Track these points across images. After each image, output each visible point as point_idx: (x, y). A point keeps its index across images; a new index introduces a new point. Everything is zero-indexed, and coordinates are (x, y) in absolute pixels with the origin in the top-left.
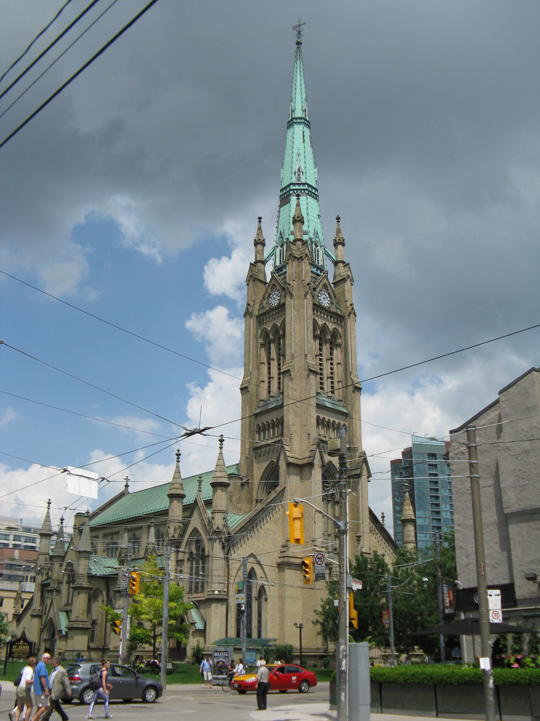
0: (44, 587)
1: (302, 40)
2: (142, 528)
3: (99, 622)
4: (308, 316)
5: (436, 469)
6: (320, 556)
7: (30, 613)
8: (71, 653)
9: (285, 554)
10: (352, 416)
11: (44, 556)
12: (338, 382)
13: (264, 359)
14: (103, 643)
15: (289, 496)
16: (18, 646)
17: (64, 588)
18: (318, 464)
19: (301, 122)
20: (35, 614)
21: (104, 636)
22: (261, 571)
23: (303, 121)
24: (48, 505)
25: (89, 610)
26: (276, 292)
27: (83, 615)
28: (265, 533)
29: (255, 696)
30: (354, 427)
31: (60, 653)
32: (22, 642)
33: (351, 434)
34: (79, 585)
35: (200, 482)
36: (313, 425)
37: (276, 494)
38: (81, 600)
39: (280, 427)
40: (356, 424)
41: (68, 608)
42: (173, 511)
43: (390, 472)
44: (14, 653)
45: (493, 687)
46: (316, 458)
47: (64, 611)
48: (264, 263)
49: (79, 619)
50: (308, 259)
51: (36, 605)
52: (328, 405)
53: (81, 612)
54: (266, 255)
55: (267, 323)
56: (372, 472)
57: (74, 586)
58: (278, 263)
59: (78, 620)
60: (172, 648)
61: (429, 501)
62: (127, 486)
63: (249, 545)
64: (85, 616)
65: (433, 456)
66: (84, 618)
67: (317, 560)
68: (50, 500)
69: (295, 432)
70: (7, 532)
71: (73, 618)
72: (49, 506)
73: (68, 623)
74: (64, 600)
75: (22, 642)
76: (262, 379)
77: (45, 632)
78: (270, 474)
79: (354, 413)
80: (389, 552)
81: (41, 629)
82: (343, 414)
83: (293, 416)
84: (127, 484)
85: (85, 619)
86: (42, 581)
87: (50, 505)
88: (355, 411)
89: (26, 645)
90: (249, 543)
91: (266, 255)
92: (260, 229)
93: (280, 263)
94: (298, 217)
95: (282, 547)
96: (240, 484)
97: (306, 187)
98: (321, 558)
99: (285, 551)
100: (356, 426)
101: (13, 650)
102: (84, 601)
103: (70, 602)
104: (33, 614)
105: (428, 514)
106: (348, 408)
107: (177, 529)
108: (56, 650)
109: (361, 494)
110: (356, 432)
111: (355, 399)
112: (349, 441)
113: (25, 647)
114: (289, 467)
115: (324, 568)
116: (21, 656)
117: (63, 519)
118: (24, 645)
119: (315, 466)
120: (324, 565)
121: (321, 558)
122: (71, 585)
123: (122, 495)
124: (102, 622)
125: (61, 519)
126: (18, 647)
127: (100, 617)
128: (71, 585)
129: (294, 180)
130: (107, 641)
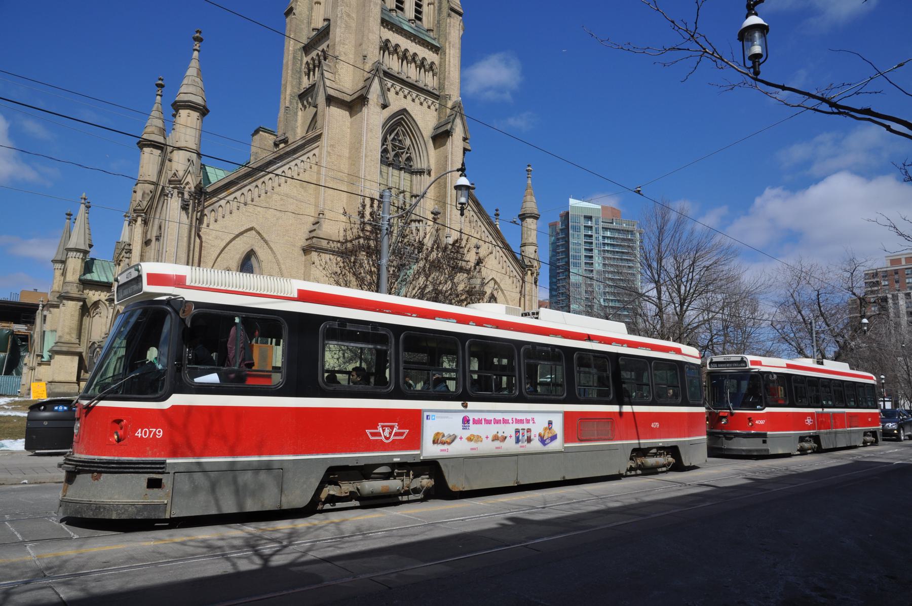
5: (591, 221)
9: (314, 234)
10: (445, 51)
15: (327, 147)
18: (375, 100)
22: (271, 257)
27: (69, 334)
28: (282, 199)
29: (890, 408)
30: (447, 66)
33: (442, 76)
36: (372, 44)
37: (304, 141)
40: (450, 62)
42: (142, 167)
43: (631, 411)
45: (622, 372)
46: (372, 89)
49: (63, 340)
52: (406, 28)
53: (67, 330)
61: (583, 260)
63: (247, 214)
65: (589, 218)
69: (344, 53)
80: (508, 268)
82: (419, 42)
83: (343, 30)
90: (246, 211)
95: (313, 225)
96: (271, 143)
99: (315, 230)
100: (449, 65)
102: (72, 315)
105: (581, 272)
106: (441, 40)
107: (148, 194)
109: (452, 160)
110: (449, 73)
111: (450, 26)
112: (439, 88)
114: (330, 103)
119: (371, 102)
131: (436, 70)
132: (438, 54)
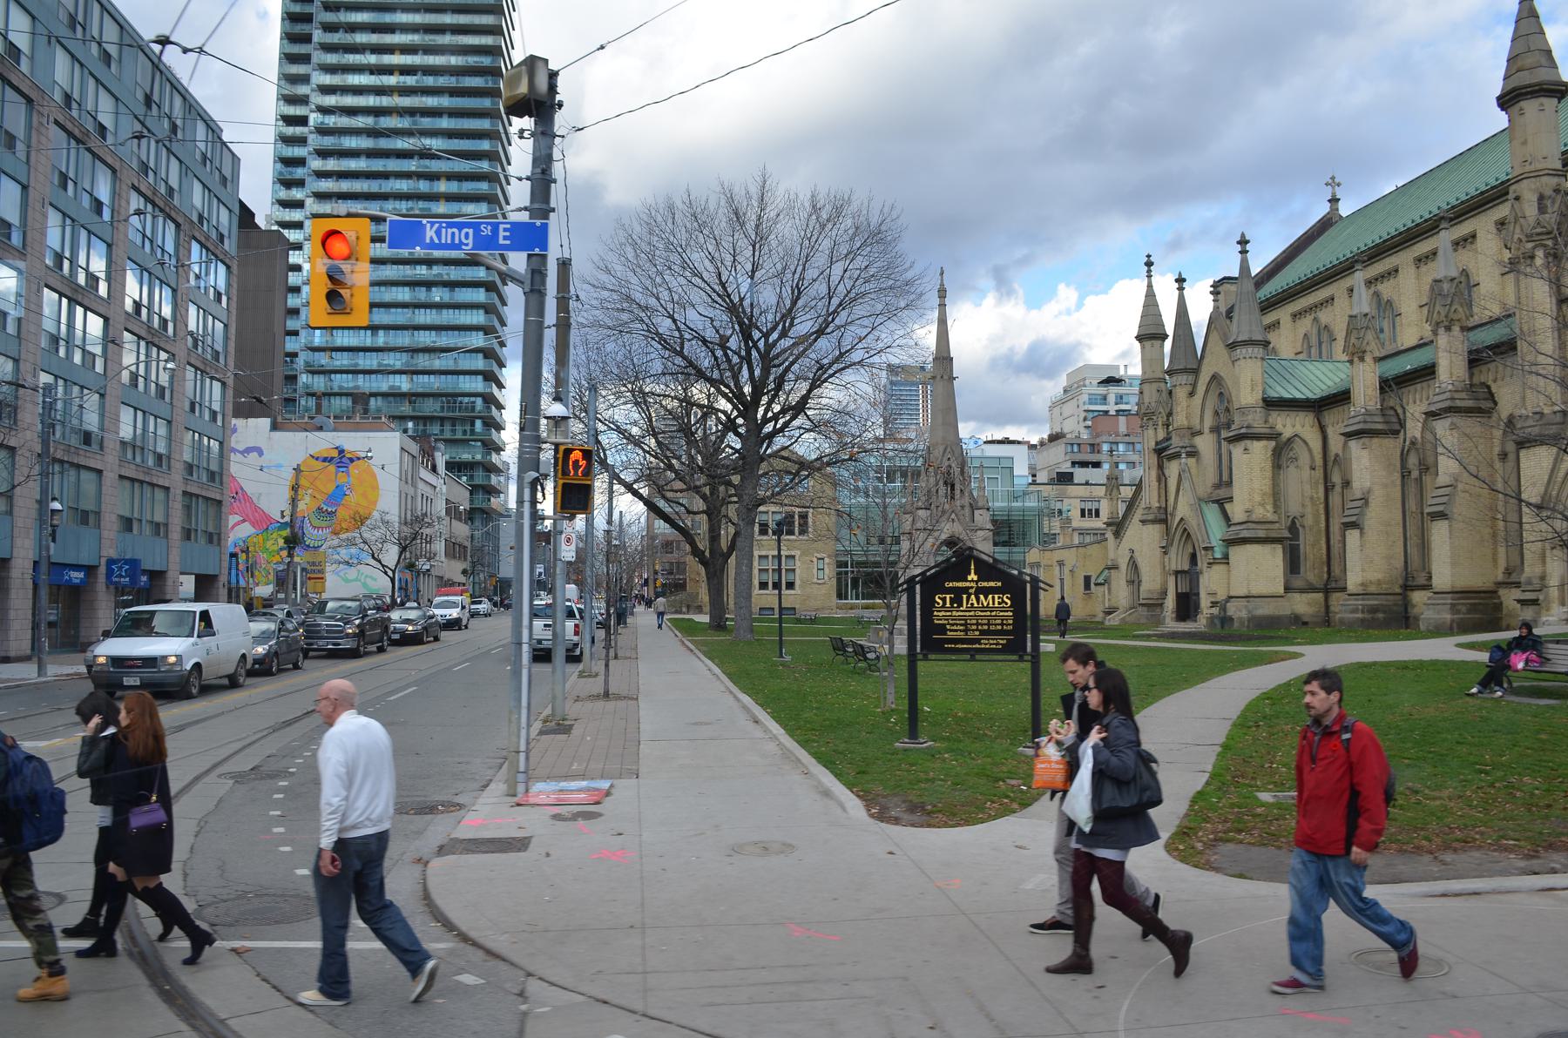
0: (1162, 452)
3: (1309, 521)
7: (1138, 514)
8: (1243, 602)
11: (1155, 386)
14: (1325, 576)
16: (958, 595)
17: (1205, 443)
20: (1151, 517)
21: (1325, 556)
25: (1276, 495)
27: (1262, 505)
31: (1214, 604)
32: (973, 576)
34: (1243, 431)
38: (1251, 463)
41: (1222, 493)
44: (942, 629)
47: (1214, 502)
49: (1254, 517)
51: (1150, 497)
53: (1258, 498)
57: (1231, 434)
59: (1250, 519)
60: (1182, 593)
64: (1270, 507)
66: (1265, 512)
68: (1149, 256)
70: (1102, 390)
71: (1237, 511)
73: (1225, 529)
74: (1211, 476)
75: (973, 576)
77: (1173, 551)
81: (1163, 547)
84: (1334, 195)
85: (1270, 516)
86: (1157, 443)
89: (993, 591)
101: (940, 616)
102: (1262, 469)
103: (1225, 478)
104: (1145, 517)
108: (1203, 595)
113: (993, 600)
116: (978, 641)
117: (1184, 280)
118: (987, 592)
122: (1224, 434)
123: (1325, 225)
124: (1317, 522)
125: (1177, 281)
126: (957, 600)
127: (1309, 510)
128: (1224, 434)
130: (1336, 570)
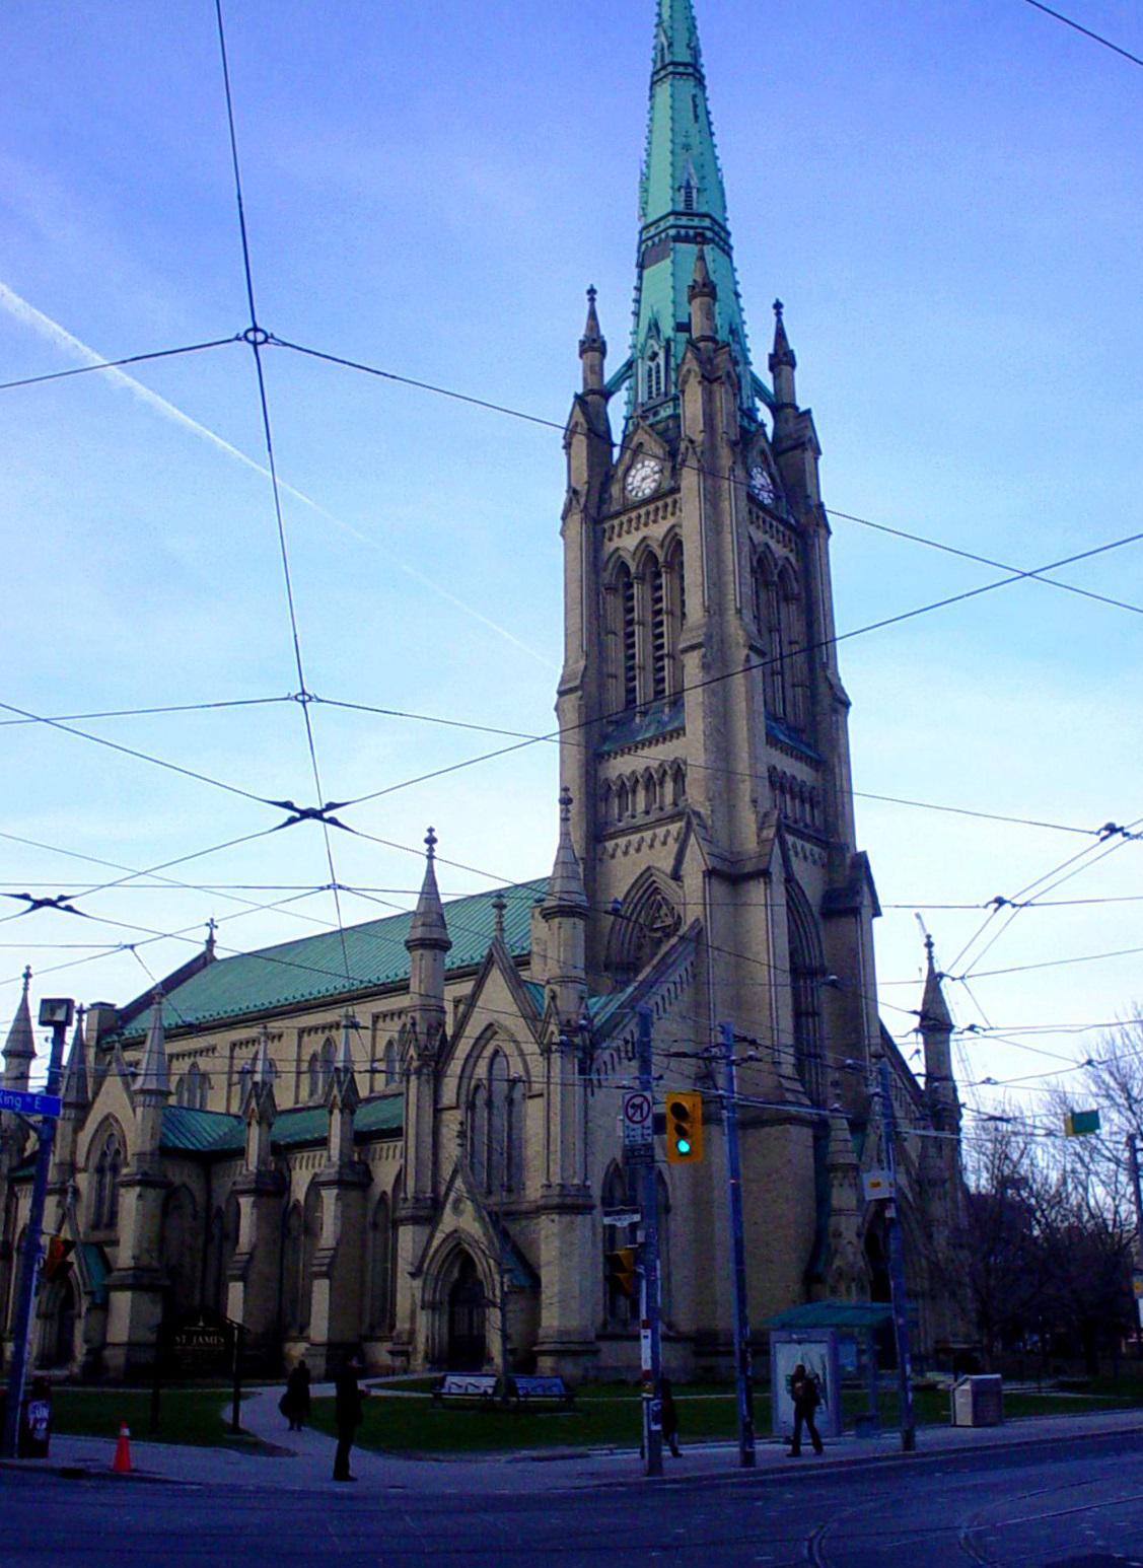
1: (926, 950)
2: (280, 1036)
4: (740, 518)
6: (638, 1101)
12: (794, 686)
13: (617, 621)
19: (688, 74)
23: (690, 70)
24: (427, 846)
26: (646, 463)
35: (500, 907)
39: (669, 786)
48: (606, 394)
50: (732, 386)
54: (610, 372)
55: (625, 536)
56: (881, 902)
58: (642, 397)
62: (211, 942)
67: (631, 1111)
72: (431, 850)
76: (612, 669)
78: (646, 896)
79: (836, 760)
87: (435, 846)
88: (839, 757)
91: (610, 372)
92: (593, 315)
93: (650, 398)
94: (704, 285)
97: (707, 223)
98: (640, 1107)
115: (650, 1131)
120: (649, 1122)
121: (640, 1107)
129: (681, 207)
131: (815, 799)
132: (817, 771)
